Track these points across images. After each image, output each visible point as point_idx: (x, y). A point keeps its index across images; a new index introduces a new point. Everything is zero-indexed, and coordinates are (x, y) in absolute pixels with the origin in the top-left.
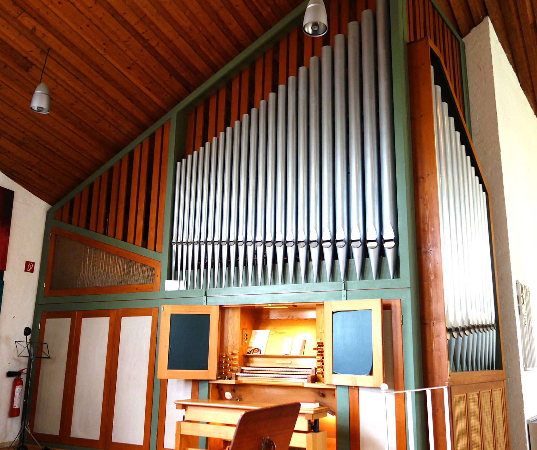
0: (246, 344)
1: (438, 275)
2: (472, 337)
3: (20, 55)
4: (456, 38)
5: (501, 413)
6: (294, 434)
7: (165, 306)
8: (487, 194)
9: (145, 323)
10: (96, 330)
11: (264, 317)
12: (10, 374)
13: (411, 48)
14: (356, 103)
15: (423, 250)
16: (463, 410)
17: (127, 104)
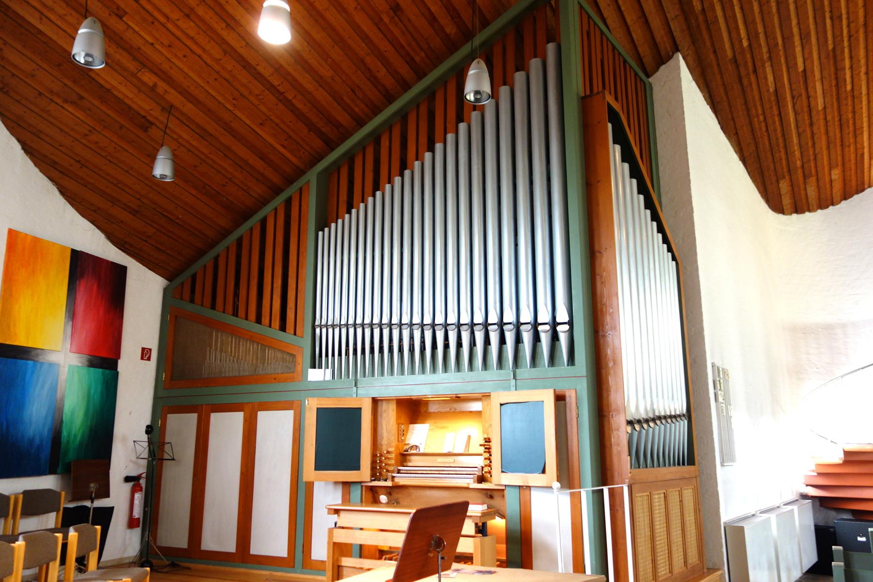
0: (403, 441)
1: (617, 362)
2: (657, 429)
3: (139, 114)
4: (641, 80)
5: (692, 514)
6: (461, 539)
7: (310, 399)
8: (677, 264)
9: (287, 417)
10: (227, 428)
11: (423, 410)
12: (128, 479)
13: (585, 102)
14: (524, 173)
15: (601, 333)
16: (646, 510)
17: (259, 164)
